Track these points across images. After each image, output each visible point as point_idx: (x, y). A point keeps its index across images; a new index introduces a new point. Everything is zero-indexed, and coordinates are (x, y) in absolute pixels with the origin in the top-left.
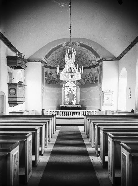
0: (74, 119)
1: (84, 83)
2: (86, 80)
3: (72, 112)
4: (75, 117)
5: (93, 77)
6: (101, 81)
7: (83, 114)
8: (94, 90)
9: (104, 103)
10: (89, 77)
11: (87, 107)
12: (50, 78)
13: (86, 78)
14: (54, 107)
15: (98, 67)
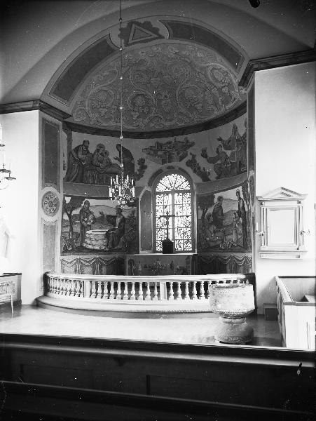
2: (219, 162)
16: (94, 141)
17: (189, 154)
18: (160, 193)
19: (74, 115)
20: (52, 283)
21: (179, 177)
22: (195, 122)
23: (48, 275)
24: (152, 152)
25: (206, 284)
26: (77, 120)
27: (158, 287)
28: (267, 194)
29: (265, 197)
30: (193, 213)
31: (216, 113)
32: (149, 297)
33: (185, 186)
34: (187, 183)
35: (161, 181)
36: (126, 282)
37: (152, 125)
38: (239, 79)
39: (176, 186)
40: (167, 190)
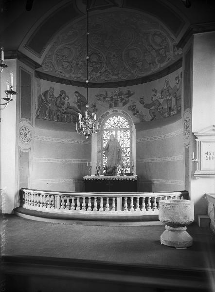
0: (100, 223)
1: (148, 118)
2: (153, 108)
3: (87, 198)
4: (101, 213)
5: (171, 99)
6: (188, 102)
7: (126, 205)
8: (174, 131)
9: (196, 172)
10: (161, 101)
11: (156, 182)
12: (61, 108)
13: (153, 104)
14: (72, 186)
15: (181, 70)
16: (58, 87)
17: (130, 101)
18: (106, 130)
19: (43, 66)
20: (26, 197)
21: (121, 118)
22: (136, 77)
23: (24, 190)
24: (102, 98)
25: (141, 199)
26: (45, 70)
27: (116, 200)
28: (202, 130)
29: (200, 133)
30: (131, 145)
31: (152, 69)
32: (108, 209)
33: (126, 124)
34: (127, 123)
35: (107, 121)
36: (96, 197)
37: (102, 78)
38: (177, 42)
39: (119, 125)
40: (112, 127)
